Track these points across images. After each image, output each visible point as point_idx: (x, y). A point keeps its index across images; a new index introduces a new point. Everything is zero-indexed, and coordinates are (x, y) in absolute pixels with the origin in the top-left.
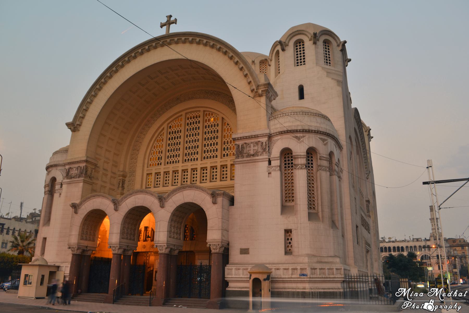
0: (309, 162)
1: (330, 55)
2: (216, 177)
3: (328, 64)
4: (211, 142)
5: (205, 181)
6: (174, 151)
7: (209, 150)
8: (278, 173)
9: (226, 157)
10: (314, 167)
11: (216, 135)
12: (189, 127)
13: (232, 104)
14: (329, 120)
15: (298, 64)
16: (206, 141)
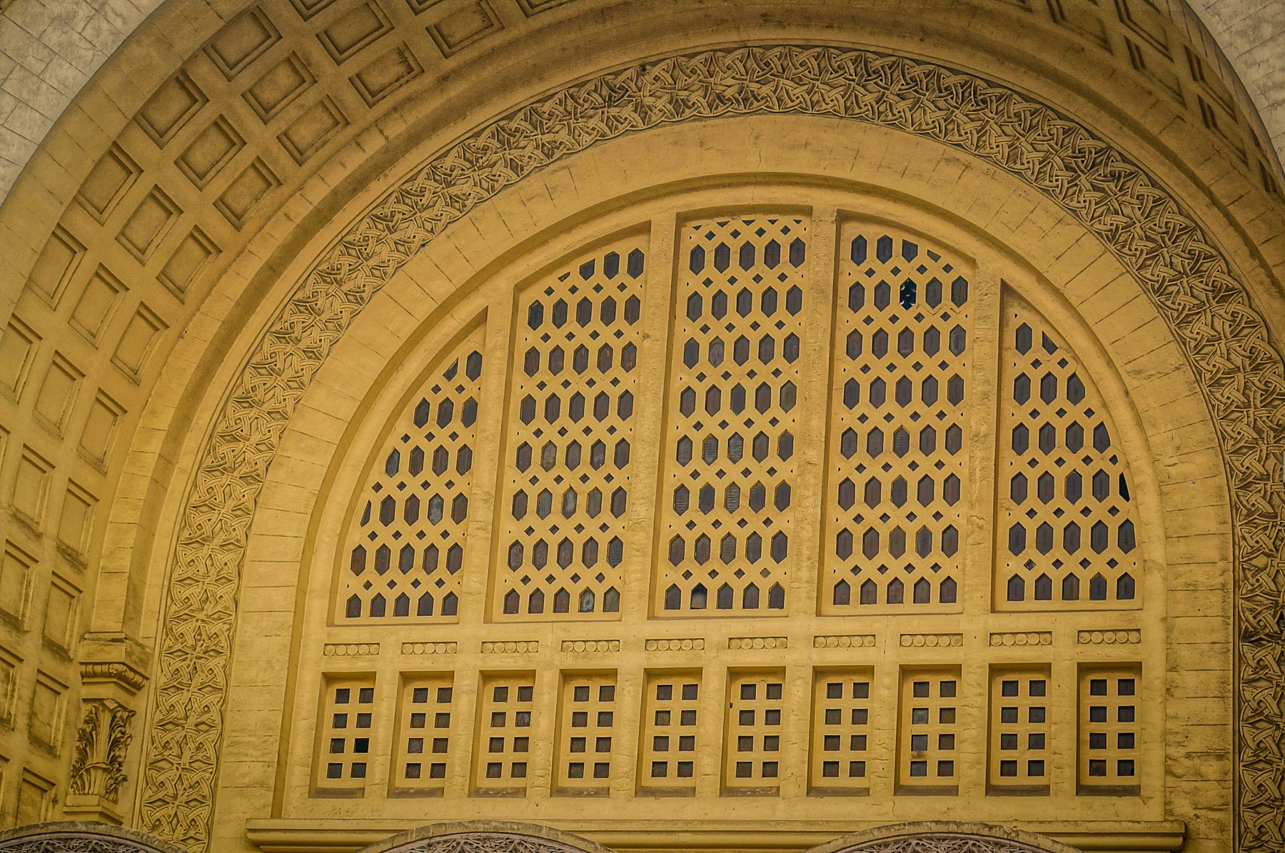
4: (900, 467)
7: (884, 531)
9: (935, 604)
13: (1095, 188)
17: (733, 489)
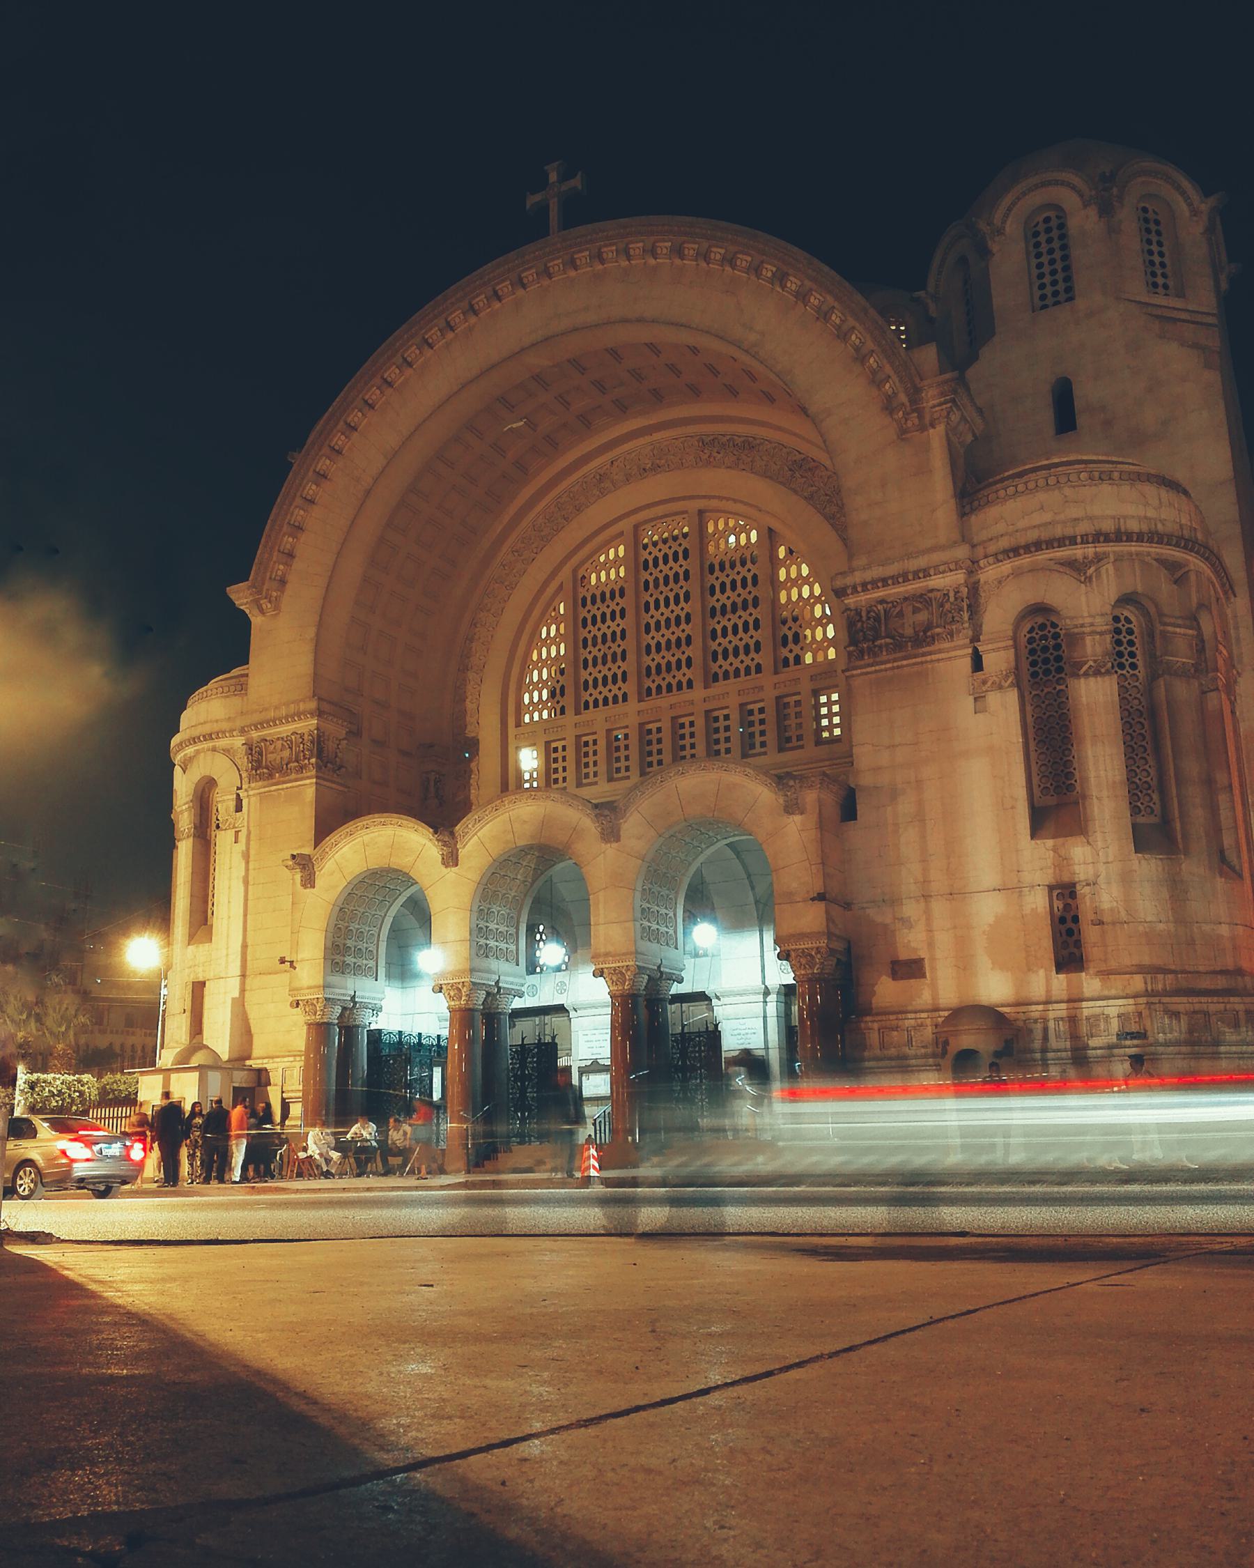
0: (1122, 648)
1: (1167, 255)
2: (763, 739)
3: (1160, 290)
5: (623, 773)
6: (604, 664)
8: (1012, 697)
10: (1140, 664)
11: (750, 593)
12: (651, 574)
13: (802, 477)
14: (1186, 493)
15: (1046, 302)
16: (716, 619)
17: (669, 641)
